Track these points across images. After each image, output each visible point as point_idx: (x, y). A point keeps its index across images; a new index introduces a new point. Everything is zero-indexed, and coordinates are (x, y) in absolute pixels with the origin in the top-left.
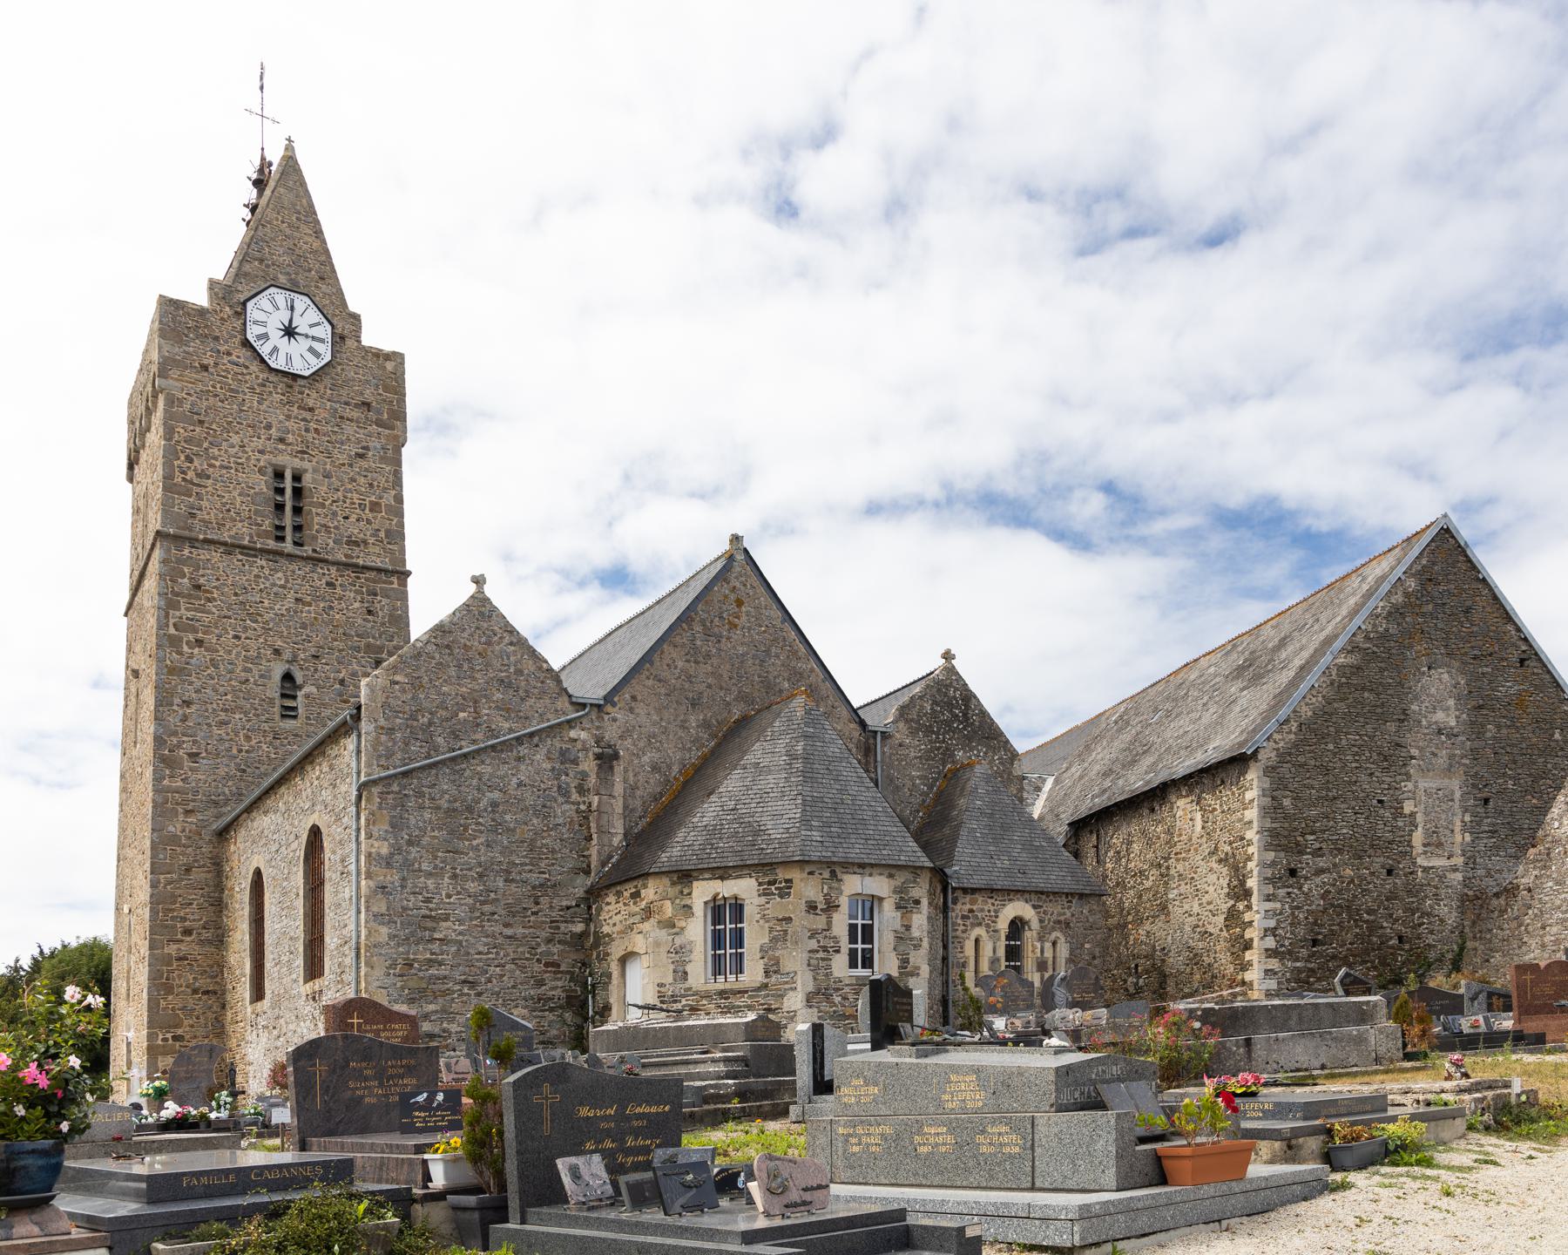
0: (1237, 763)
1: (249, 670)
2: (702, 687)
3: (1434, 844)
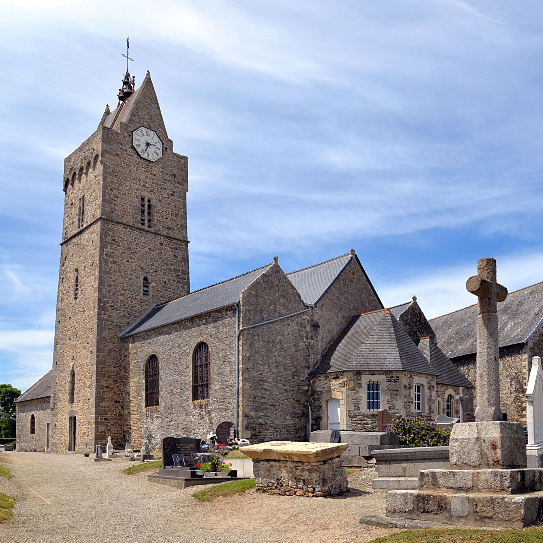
0: (232, 308)
2: (343, 303)
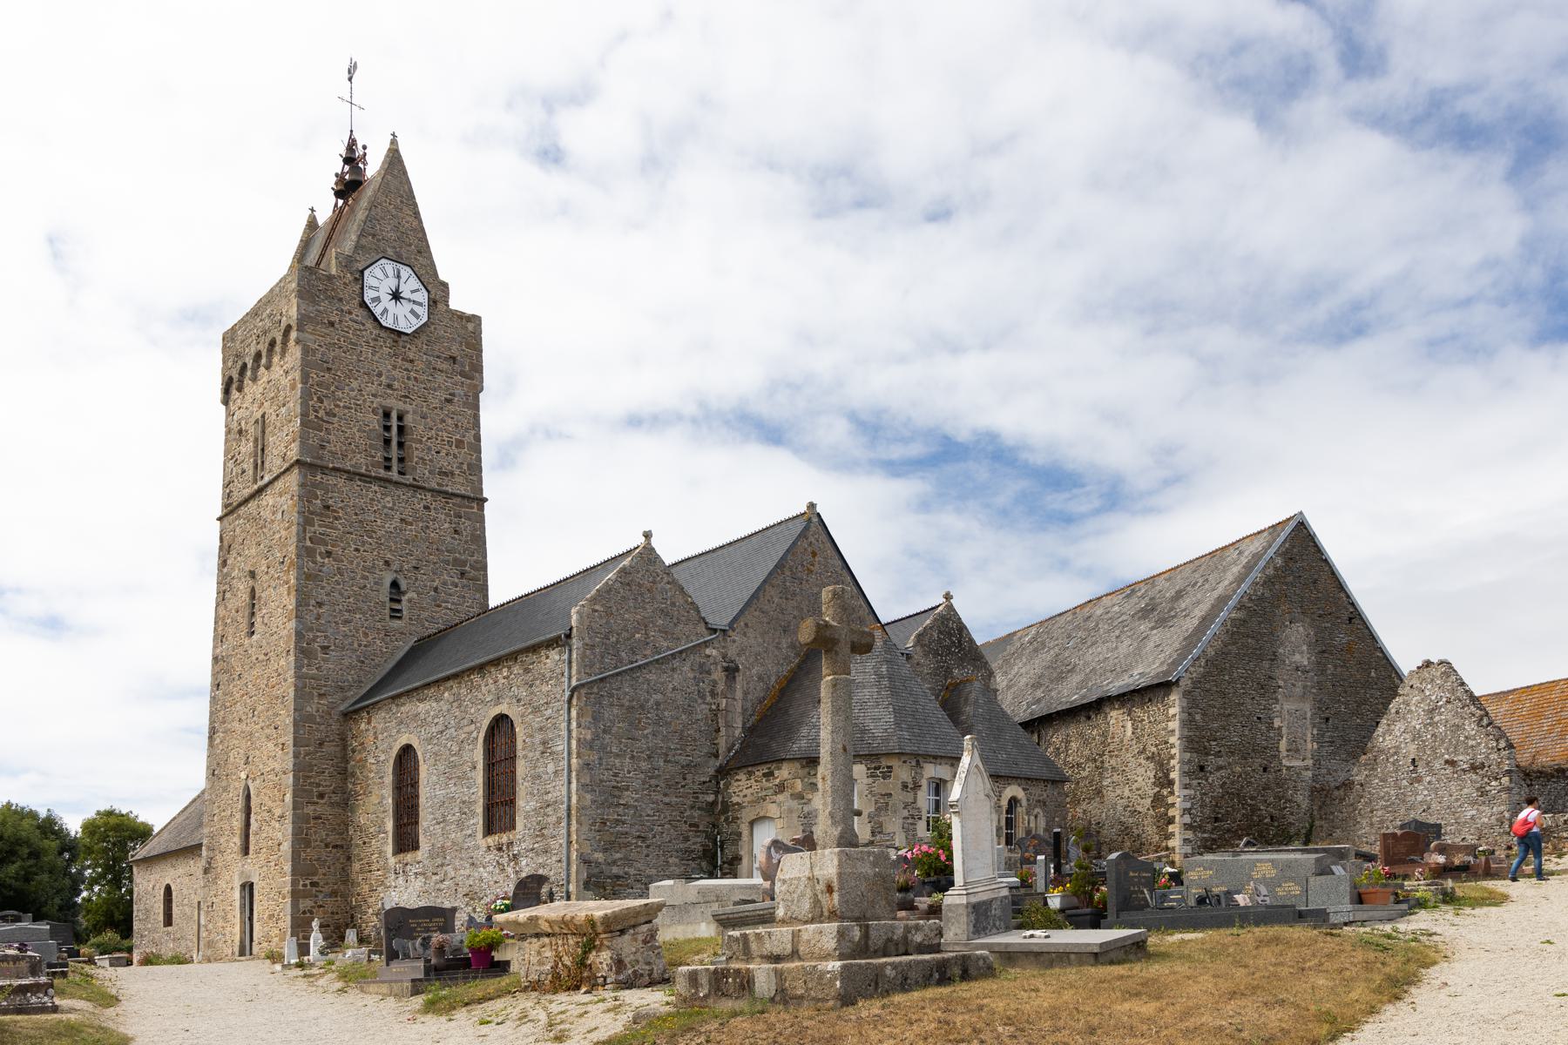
0: (1162, 687)
1: (366, 578)
3: (1294, 750)
